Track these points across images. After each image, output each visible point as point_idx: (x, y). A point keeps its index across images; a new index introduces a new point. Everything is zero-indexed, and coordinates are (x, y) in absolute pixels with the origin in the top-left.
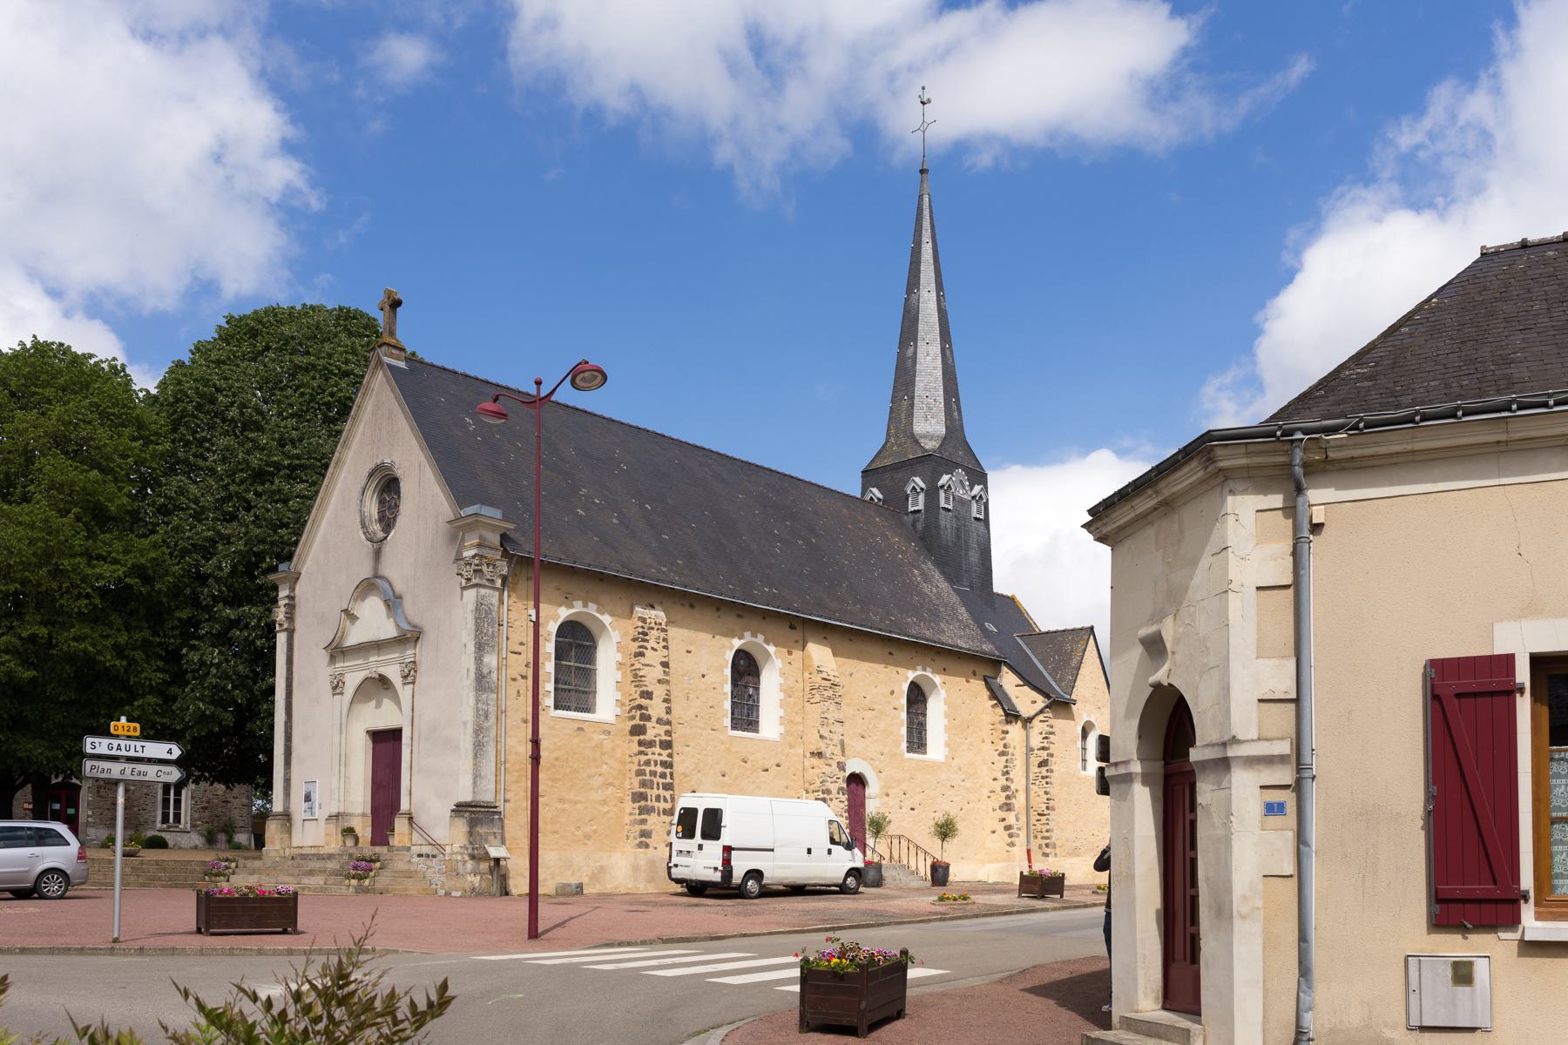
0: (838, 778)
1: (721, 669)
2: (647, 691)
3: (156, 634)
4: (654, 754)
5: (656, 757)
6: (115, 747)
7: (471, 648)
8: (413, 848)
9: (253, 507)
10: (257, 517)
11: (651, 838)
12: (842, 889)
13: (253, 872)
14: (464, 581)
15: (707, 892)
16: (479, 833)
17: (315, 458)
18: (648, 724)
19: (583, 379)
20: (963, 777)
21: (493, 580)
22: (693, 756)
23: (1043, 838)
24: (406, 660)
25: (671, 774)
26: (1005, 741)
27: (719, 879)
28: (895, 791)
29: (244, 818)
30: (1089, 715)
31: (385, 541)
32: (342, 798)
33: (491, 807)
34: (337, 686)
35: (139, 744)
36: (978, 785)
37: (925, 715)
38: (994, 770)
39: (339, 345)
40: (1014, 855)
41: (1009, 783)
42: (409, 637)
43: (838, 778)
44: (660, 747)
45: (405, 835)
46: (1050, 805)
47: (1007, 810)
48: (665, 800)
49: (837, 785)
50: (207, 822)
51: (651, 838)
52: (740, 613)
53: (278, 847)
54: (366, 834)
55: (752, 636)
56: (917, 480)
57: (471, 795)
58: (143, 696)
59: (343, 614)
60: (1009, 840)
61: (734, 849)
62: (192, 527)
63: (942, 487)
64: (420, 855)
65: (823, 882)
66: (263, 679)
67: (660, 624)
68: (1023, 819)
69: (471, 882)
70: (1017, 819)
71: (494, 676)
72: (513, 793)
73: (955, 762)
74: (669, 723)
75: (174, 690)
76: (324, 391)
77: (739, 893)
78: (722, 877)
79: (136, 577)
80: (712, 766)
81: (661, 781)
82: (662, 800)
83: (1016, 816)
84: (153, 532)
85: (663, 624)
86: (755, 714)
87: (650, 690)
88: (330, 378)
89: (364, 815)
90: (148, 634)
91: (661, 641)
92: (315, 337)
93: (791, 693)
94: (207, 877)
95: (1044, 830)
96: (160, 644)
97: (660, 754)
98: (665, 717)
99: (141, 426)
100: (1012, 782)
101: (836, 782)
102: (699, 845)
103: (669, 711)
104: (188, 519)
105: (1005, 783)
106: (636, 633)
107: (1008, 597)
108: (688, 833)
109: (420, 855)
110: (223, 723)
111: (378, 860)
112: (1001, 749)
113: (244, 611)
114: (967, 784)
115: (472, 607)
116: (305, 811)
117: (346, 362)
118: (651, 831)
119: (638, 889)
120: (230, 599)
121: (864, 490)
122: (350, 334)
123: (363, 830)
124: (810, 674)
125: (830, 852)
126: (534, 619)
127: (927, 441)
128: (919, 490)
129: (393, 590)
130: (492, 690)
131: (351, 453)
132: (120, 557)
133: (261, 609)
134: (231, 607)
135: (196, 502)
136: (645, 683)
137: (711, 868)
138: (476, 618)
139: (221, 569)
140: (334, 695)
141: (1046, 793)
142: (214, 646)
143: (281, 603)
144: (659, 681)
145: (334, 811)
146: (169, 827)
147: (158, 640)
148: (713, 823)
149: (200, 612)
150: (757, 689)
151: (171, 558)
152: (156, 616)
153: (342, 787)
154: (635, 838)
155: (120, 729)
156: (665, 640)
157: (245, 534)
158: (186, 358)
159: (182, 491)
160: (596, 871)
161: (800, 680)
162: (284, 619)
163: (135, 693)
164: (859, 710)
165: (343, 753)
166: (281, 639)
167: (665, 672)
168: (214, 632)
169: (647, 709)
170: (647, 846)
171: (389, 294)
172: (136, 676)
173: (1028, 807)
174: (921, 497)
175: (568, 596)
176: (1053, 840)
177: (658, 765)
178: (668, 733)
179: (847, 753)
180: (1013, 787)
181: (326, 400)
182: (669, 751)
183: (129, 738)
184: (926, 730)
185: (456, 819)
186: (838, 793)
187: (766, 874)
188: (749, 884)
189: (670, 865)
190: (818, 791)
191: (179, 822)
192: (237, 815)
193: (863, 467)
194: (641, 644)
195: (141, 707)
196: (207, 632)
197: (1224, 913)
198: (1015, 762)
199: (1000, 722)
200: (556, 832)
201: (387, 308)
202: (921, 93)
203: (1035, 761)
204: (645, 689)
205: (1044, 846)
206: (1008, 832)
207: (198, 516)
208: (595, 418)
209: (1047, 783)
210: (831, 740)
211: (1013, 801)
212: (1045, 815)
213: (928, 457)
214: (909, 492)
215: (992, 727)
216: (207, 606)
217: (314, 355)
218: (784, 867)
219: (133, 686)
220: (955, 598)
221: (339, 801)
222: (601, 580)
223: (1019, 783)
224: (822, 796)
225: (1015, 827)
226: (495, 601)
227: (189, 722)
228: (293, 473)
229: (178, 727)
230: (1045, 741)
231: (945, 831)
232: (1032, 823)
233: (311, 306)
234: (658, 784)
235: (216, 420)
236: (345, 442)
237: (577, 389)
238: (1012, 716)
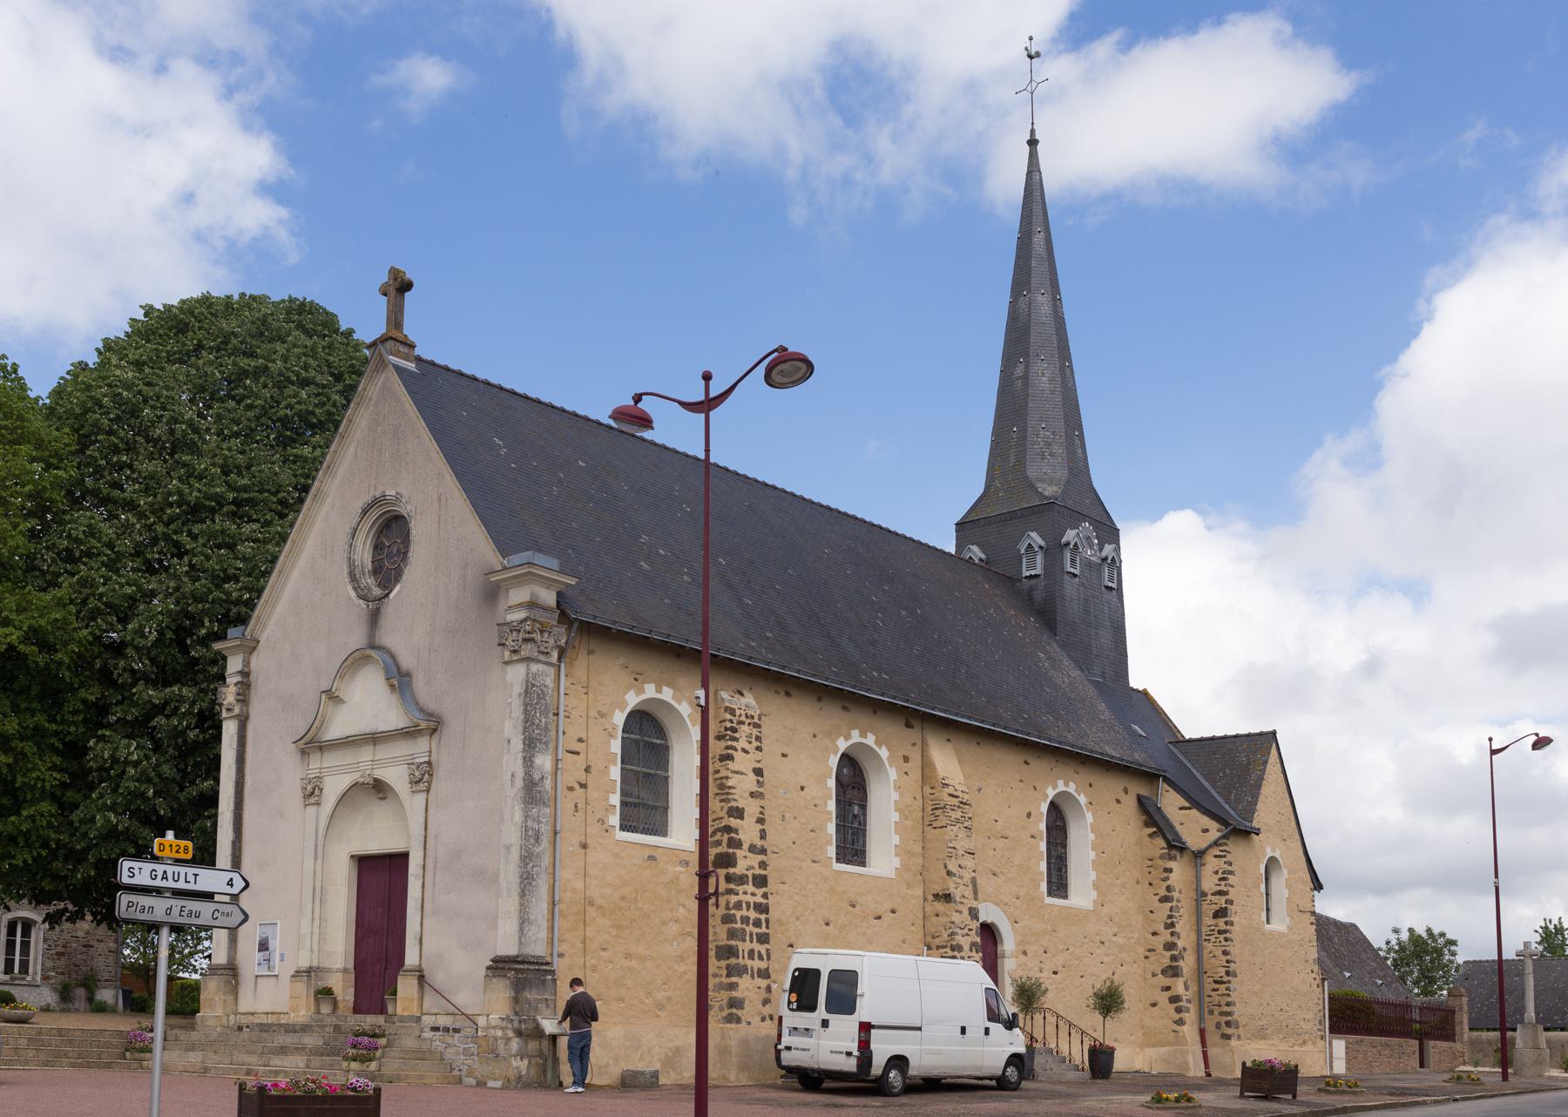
0: (971, 930)
1: (822, 780)
2: (737, 807)
3: (52, 720)
4: (745, 893)
5: (749, 898)
6: (160, 877)
7: (518, 744)
8: (425, 1018)
9: (186, 552)
10: (192, 566)
11: (743, 1009)
12: (1001, 1084)
13: (192, 1048)
14: (507, 654)
15: (825, 1085)
16: (527, 1000)
17: (269, 491)
18: (739, 853)
19: (781, 373)
20: (1115, 930)
21: (548, 653)
22: (790, 897)
23: (1222, 1014)
24: (417, 760)
25: (767, 921)
26: (1169, 883)
27: (854, 1069)
28: (1034, 948)
29: (110, 969)
30: (1273, 850)
31: (386, 600)
32: (315, 948)
33: (542, 964)
34: (313, 793)
35: (191, 871)
36: (1133, 941)
37: (1065, 846)
38: (1153, 921)
39: (295, 346)
40: (1184, 1036)
41: (1174, 939)
42: (429, 725)
43: (971, 930)
44: (754, 885)
45: (412, 1000)
46: (1231, 969)
47: (1173, 976)
48: (760, 957)
49: (969, 939)
50: (62, 973)
51: (743, 1009)
52: (846, 705)
53: (219, 1012)
54: (347, 998)
55: (861, 736)
56: (1034, 535)
57: (516, 946)
58: (33, 802)
59: (323, 697)
60: (1177, 1017)
61: (873, 1027)
62: (107, 580)
63: (1068, 544)
64: (435, 1029)
65: (978, 1074)
66: (193, 783)
67: (753, 717)
68: (1194, 988)
69: (517, 1068)
70: (1187, 989)
71: (548, 783)
72: (568, 944)
73: (1106, 910)
74: (763, 851)
75: (70, 795)
76: (278, 403)
77: (878, 1088)
78: (858, 1065)
79: (33, 644)
80: (813, 910)
81: (756, 930)
82: (756, 956)
83: (1185, 983)
84: (55, 584)
85: (756, 717)
86: (861, 841)
87: (741, 806)
88: (286, 387)
89: (345, 971)
90: (42, 719)
91: (753, 740)
92: (262, 334)
93: (908, 814)
94: (128, 1054)
95: (1223, 1003)
96: (56, 733)
97: (753, 894)
98: (759, 843)
99: (39, 444)
100: (1179, 938)
101: (967, 935)
102: (823, 1020)
103: (763, 835)
104: (99, 568)
105: (1169, 939)
106: (723, 729)
107: (1139, 691)
108: (806, 1003)
109: (435, 1029)
110: (140, 842)
111: (383, 1036)
112: (1163, 892)
113: (173, 692)
114: (1120, 940)
115: (518, 689)
116: (259, 964)
117: (306, 367)
118: (744, 999)
119: (728, 1080)
120: (153, 676)
121: (959, 546)
122: (309, 334)
123: (343, 991)
124: (932, 788)
125: (987, 1031)
126: (703, 703)
127: (1045, 485)
128: (1036, 549)
129: (397, 665)
130: (544, 803)
131: (336, 482)
132: (14, 616)
133: (195, 690)
134: (155, 688)
135: (110, 545)
136: (735, 797)
137: (841, 1053)
138: (526, 705)
139: (143, 636)
140: (306, 805)
141: (1225, 953)
142: (130, 736)
143: (231, 680)
144: (752, 795)
145: (304, 964)
146: (13, 979)
147: (54, 727)
148: (844, 992)
149: (111, 691)
150: (863, 807)
151: (77, 620)
152: (52, 694)
153: (316, 930)
154: (722, 1009)
155: (168, 849)
156: (758, 739)
157: (177, 589)
158: (92, 359)
159: (92, 532)
160: (670, 1054)
161: (919, 796)
162: (234, 702)
163: (21, 798)
164: (989, 838)
165: (318, 885)
166: (229, 729)
167: (758, 781)
168: (129, 718)
169: (736, 832)
170: (738, 1020)
171: (395, 274)
172: (24, 775)
173: (1200, 972)
174: (1039, 559)
175: (637, 677)
176: (1235, 1017)
177: (751, 909)
178: (763, 865)
179: (980, 896)
180: (1180, 944)
181: (282, 413)
182: (764, 889)
183: (178, 861)
184: (1066, 866)
185: (494, 980)
186: (971, 950)
187: (913, 1062)
188: (891, 1075)
189: (779, 1047)
190: (945, 947)
191: (27, 972)
192: (102, 963)
193: (958, 518)
194: (730, 743)
195: (32, 818)
196: (119, 719)
197: (185, 1018)
198: (1181, 910)
199: (1161, 857)
200: (621, 999)
201: (392, 292)
202: (1028, 45)
203: (1208, 910)
204: (734, 804)
205: (1224, 1025)
206: (1175, 1005)
207: (113, 566)
208: (645, 444)
209: (1226, 940)
210: (961, 877)
211: (1181, 963)
212: (1224, 983)
213: (1049, 505)
214: (1022, 552)
215: (1149, 863)
216: (124, 685)
217: (262, 357)
218: (934, 1053)
219: (19, 788)
220: (1091, 691)
221: (312, 951)
222: (678, 656)
223: (1186, 940)
224: (950, 953)
225: (1184, 998)
226: (549, 682)
227: (94, 839)
228: (240, 509)
229: (78, 847)
230: (1223, 883)
231: (1108, 1002)
232: (1206, 994)
233: (251, 296)
234: (751, 935)
235: (138, 438)
236: (329, 467)
237: (771, 386)
238: (1176, 846)
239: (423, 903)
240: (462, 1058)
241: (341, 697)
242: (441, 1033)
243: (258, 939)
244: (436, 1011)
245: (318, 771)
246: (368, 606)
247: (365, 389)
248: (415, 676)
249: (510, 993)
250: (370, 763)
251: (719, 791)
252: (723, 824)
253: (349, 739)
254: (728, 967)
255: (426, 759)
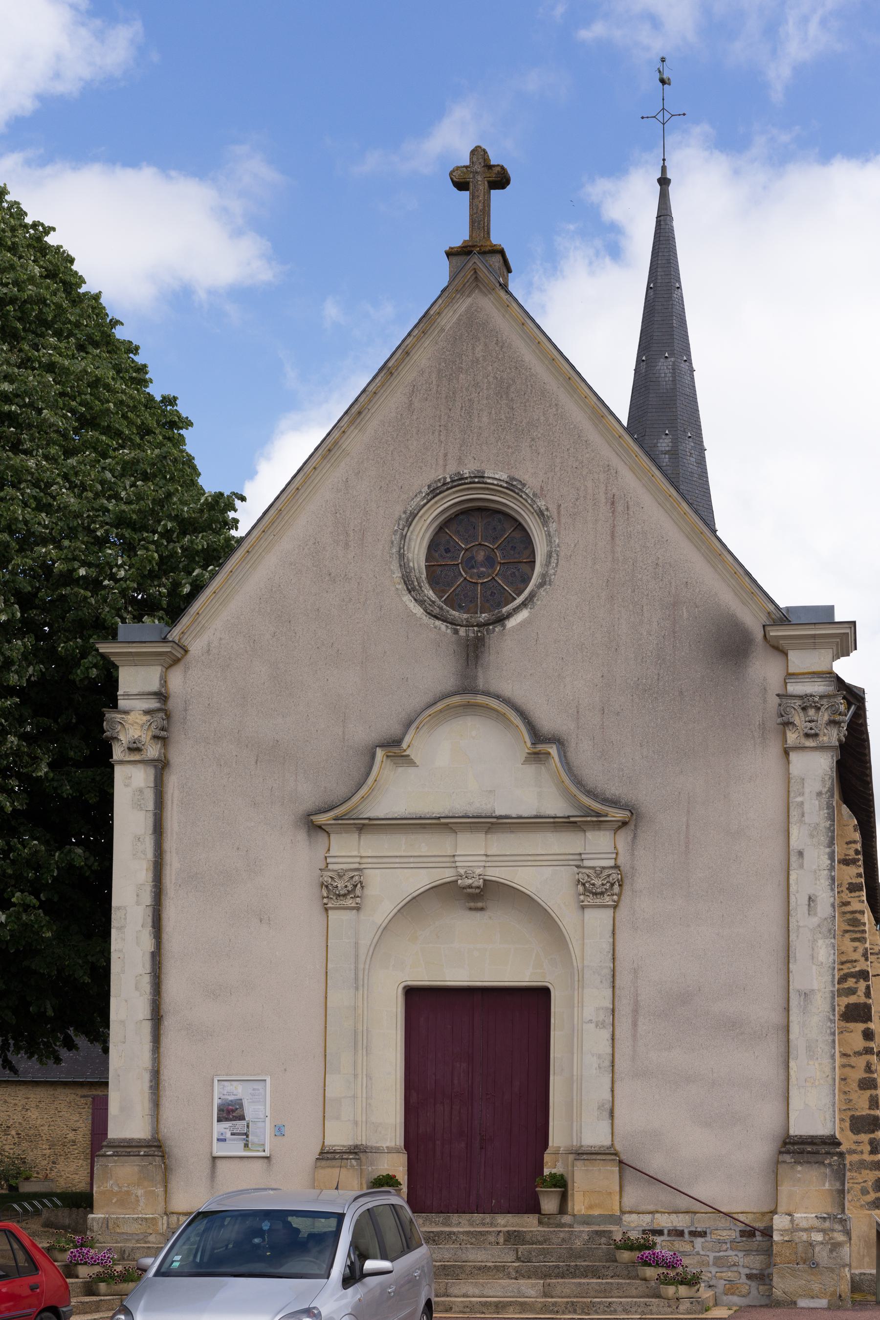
8: (626, 1218)
154: (865, 1192)
185: (799, 1168)
236: (360, 413)
239: (613, 1062)
240: (714, 1270)
241: (412, 757)
242: (665, 1237)
243: (216, 1102)
244: (651, 1208)
245: (358, 860)
246: (456, 632)
247: (439, 314)
248: (573, 745)
249: (831, 1185)
250: (484, 858)
251: (849, 928)
252: (857, 969)
253: (443, 821)
254: (871, 1142)
255: (611, 863)
